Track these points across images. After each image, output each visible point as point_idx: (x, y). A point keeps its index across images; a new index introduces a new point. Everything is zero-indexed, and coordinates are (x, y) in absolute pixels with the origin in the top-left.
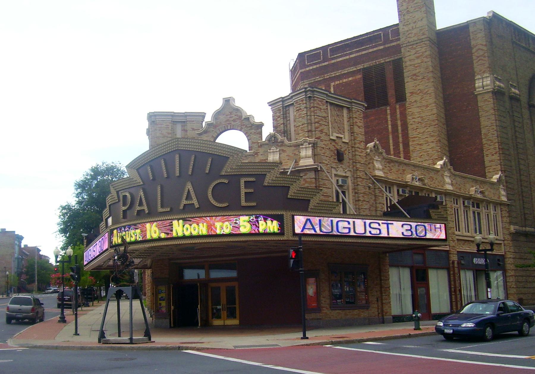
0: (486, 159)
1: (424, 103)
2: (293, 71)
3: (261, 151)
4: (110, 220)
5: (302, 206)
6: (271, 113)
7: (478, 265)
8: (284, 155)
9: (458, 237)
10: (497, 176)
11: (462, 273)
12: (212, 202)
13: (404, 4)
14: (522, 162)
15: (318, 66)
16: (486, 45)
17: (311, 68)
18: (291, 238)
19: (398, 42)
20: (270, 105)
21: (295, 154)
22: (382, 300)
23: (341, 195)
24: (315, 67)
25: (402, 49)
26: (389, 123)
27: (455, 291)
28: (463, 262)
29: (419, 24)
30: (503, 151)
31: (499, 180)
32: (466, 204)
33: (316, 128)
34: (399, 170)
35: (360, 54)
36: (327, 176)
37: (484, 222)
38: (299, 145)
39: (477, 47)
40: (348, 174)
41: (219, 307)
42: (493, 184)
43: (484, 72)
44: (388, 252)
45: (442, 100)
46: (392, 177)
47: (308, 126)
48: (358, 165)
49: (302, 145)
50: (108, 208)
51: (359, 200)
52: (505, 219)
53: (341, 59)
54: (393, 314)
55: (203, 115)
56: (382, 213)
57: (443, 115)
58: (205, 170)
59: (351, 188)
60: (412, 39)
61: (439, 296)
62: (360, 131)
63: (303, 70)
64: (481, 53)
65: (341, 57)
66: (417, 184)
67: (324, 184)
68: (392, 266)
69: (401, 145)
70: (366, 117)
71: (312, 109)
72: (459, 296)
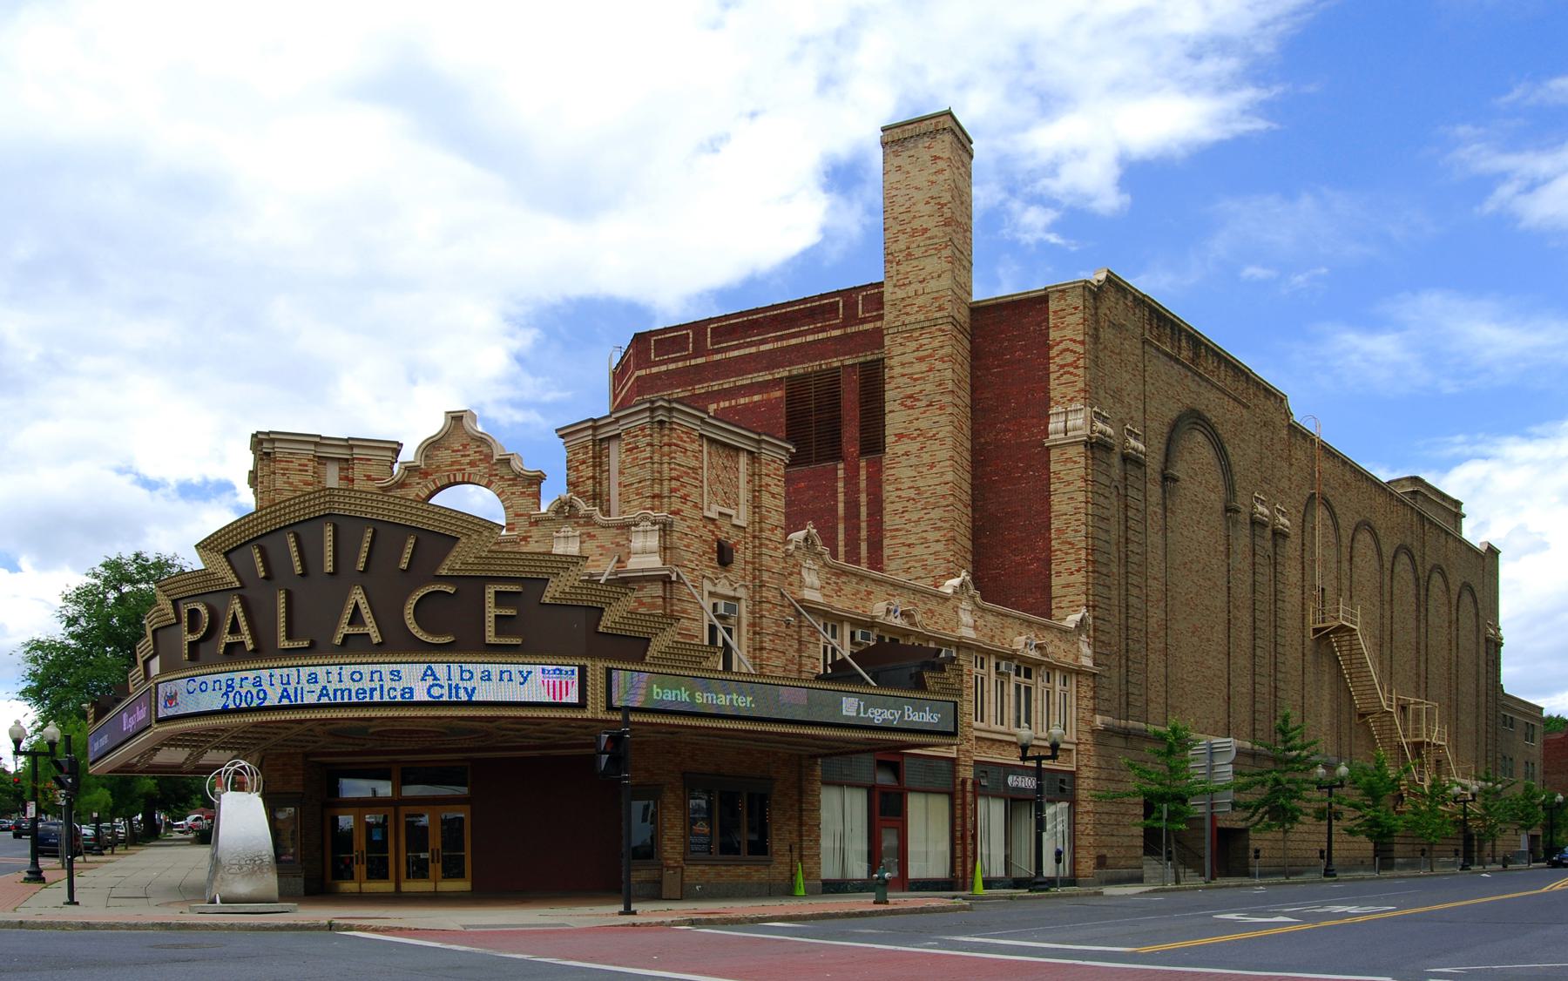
0: (1055, 581)
1: (926, 458)
2: (619, 374)
3: (536, 532)
4: (155, 666)
5: (630, 647)
6: (563, 454)
7: (1017, 789)
8: (590, 546)
9: (977, 734)
10: (1078, 617)
11: (981, 803)
12: (411, 627)
13: (901, 237)
14: (1135, 591)
15: (680, 364)
16: (1083, 343)
17: (664, 368)
18: (600, 716)
19: (878, 324)
20: (562, 437)
21: (618, 545)
22: (801, 849)
23: (721, 633)
24: (672, 366)
25: (887, 339)
26: (841, 497)
27: (963, 839)
28: (984, 782)
29: (933, 285)
30: (1096, 564)
31: (1081, 624)
32: (1003, 668)
33: (672, 490)
34: (858, 592)
35: (785, 343)
36: (693, 596)
37: (1038, 705)
38: (629, 526)
39: (1062, 346)
40: (741, 593)
41: (422, 855)
42: (1065, 631)
43: (1071, 400)
44: (820, 756)
45: (967, 455)
46: (841, 604)
47: (652, 486)
48: (765, 576)
49: (636, 525)
50: (150, 637)
51: (762, 649)
52: (1084, 703)
53: (736, 353)
54: (823, 877)
55: (396, 448)
56: (812, 677)
57: (966, 487)
58: (399, 562)
59: (744, 623)
60: (912, 319)
61: (928, 847)
62: (775, 507)
63: (643, 372)
64: (1070, 358)
65: (737, 347)
66: (899, 622)
67: (684, 611)
68: (828, 783)
69: (864, 547)
70: (788, 480)
71: (666, 449)
72: (970, 848)
